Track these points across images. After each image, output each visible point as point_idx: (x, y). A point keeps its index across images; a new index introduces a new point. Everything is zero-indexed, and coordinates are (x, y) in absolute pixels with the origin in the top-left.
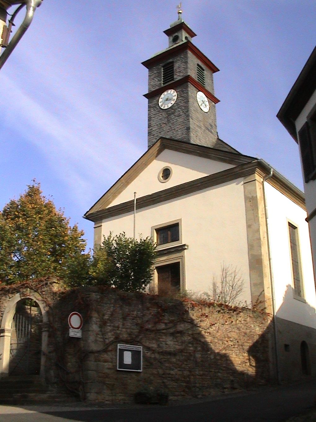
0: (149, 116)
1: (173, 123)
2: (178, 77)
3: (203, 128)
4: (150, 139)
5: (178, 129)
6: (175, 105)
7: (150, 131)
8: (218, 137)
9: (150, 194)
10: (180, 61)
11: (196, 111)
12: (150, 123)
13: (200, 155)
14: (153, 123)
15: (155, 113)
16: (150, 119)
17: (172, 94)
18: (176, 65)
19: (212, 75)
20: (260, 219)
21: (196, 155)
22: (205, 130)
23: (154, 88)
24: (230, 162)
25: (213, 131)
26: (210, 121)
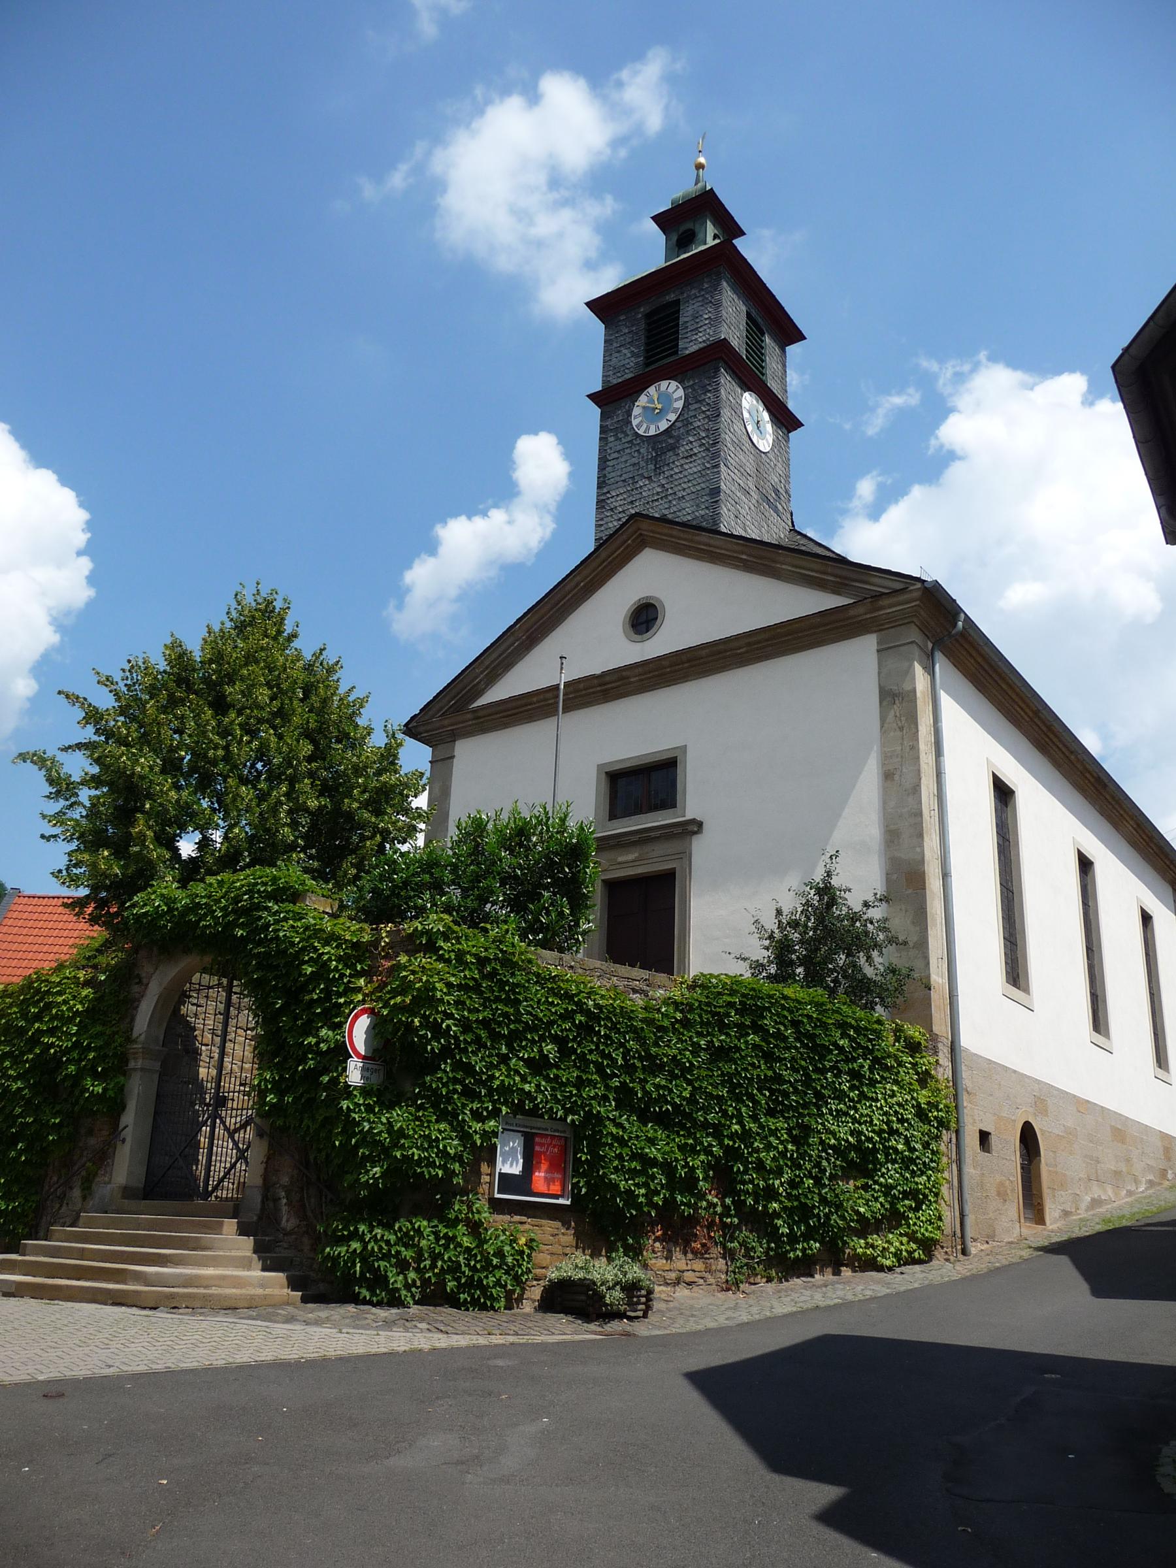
0: (604, 454)
1: (672, 476)
2: (690, 344)
3: (755, 495)
4: (602, 519)
5: (684, 494)
6: (678, 424)
7: (602, 498)
8: (793, 526)
9: (598, 672)
10: (700, 299)
11: (738, 445)
12: (605, 476)
13: (749, 567)
14: (612, 475)
15: (619, 448)
16: (603, 462)
17: (673, 390)
18: (686, 315)
19: (784, 351)
20: (922, 756)
21: (737, 567)
22: (761, 501)
23: (619, 375)
24: (836, 589)
25: (780, 507)
26: (774, 479)
